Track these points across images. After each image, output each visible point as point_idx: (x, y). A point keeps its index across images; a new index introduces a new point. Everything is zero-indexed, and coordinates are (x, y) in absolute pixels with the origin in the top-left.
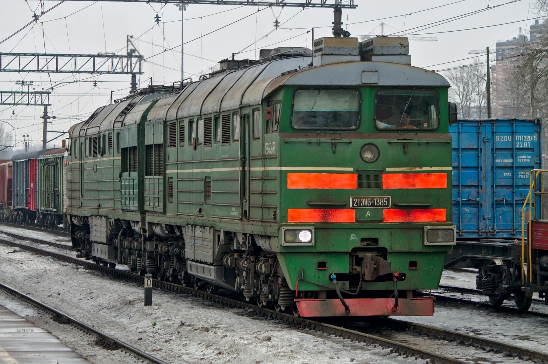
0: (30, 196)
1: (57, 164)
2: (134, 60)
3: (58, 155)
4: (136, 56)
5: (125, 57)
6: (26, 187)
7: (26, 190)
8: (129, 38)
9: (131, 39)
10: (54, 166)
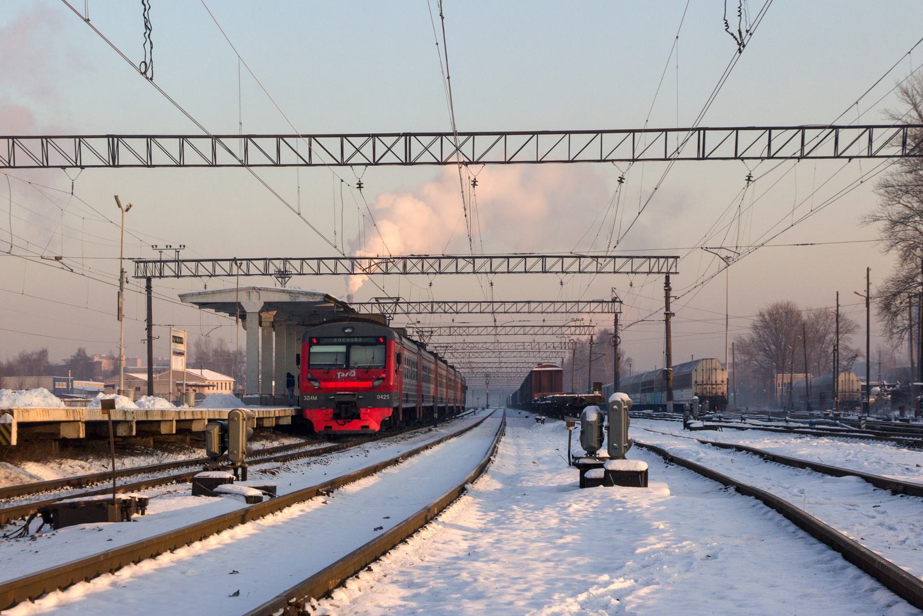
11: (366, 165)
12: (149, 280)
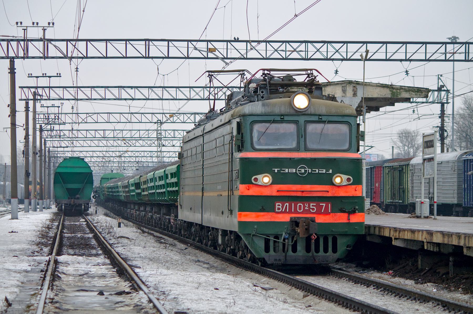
0: (375, 193)
1: (403, 169)
2: (443, 93)
3: (402, 163)
4: (444, 90)
5: (436, 91)
6: (371, 186)
7: (371, 189)
8: (440, 76)
9: (441, 78)
10: (400, 171)
11: (163, 58)
12: (12, 61)
